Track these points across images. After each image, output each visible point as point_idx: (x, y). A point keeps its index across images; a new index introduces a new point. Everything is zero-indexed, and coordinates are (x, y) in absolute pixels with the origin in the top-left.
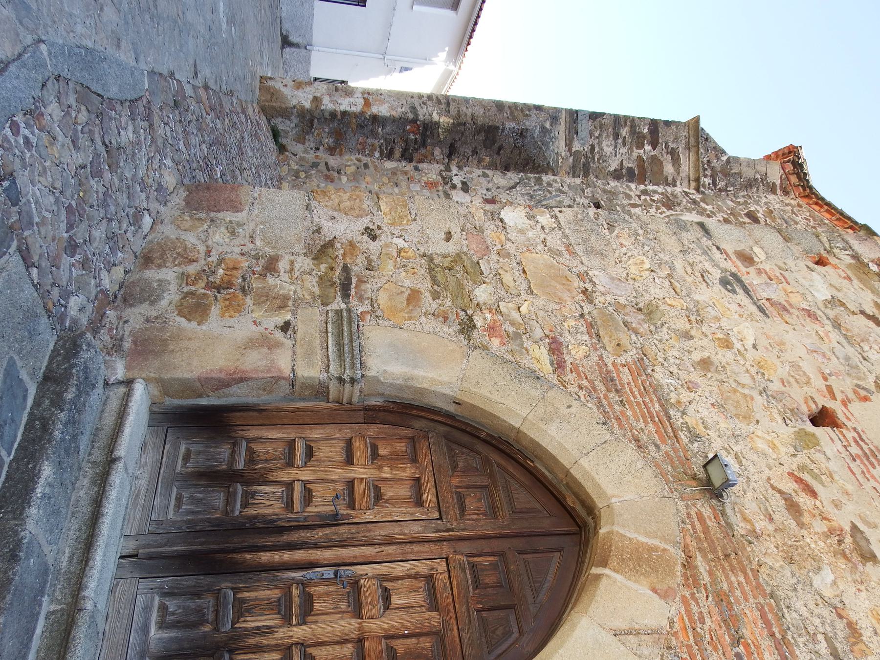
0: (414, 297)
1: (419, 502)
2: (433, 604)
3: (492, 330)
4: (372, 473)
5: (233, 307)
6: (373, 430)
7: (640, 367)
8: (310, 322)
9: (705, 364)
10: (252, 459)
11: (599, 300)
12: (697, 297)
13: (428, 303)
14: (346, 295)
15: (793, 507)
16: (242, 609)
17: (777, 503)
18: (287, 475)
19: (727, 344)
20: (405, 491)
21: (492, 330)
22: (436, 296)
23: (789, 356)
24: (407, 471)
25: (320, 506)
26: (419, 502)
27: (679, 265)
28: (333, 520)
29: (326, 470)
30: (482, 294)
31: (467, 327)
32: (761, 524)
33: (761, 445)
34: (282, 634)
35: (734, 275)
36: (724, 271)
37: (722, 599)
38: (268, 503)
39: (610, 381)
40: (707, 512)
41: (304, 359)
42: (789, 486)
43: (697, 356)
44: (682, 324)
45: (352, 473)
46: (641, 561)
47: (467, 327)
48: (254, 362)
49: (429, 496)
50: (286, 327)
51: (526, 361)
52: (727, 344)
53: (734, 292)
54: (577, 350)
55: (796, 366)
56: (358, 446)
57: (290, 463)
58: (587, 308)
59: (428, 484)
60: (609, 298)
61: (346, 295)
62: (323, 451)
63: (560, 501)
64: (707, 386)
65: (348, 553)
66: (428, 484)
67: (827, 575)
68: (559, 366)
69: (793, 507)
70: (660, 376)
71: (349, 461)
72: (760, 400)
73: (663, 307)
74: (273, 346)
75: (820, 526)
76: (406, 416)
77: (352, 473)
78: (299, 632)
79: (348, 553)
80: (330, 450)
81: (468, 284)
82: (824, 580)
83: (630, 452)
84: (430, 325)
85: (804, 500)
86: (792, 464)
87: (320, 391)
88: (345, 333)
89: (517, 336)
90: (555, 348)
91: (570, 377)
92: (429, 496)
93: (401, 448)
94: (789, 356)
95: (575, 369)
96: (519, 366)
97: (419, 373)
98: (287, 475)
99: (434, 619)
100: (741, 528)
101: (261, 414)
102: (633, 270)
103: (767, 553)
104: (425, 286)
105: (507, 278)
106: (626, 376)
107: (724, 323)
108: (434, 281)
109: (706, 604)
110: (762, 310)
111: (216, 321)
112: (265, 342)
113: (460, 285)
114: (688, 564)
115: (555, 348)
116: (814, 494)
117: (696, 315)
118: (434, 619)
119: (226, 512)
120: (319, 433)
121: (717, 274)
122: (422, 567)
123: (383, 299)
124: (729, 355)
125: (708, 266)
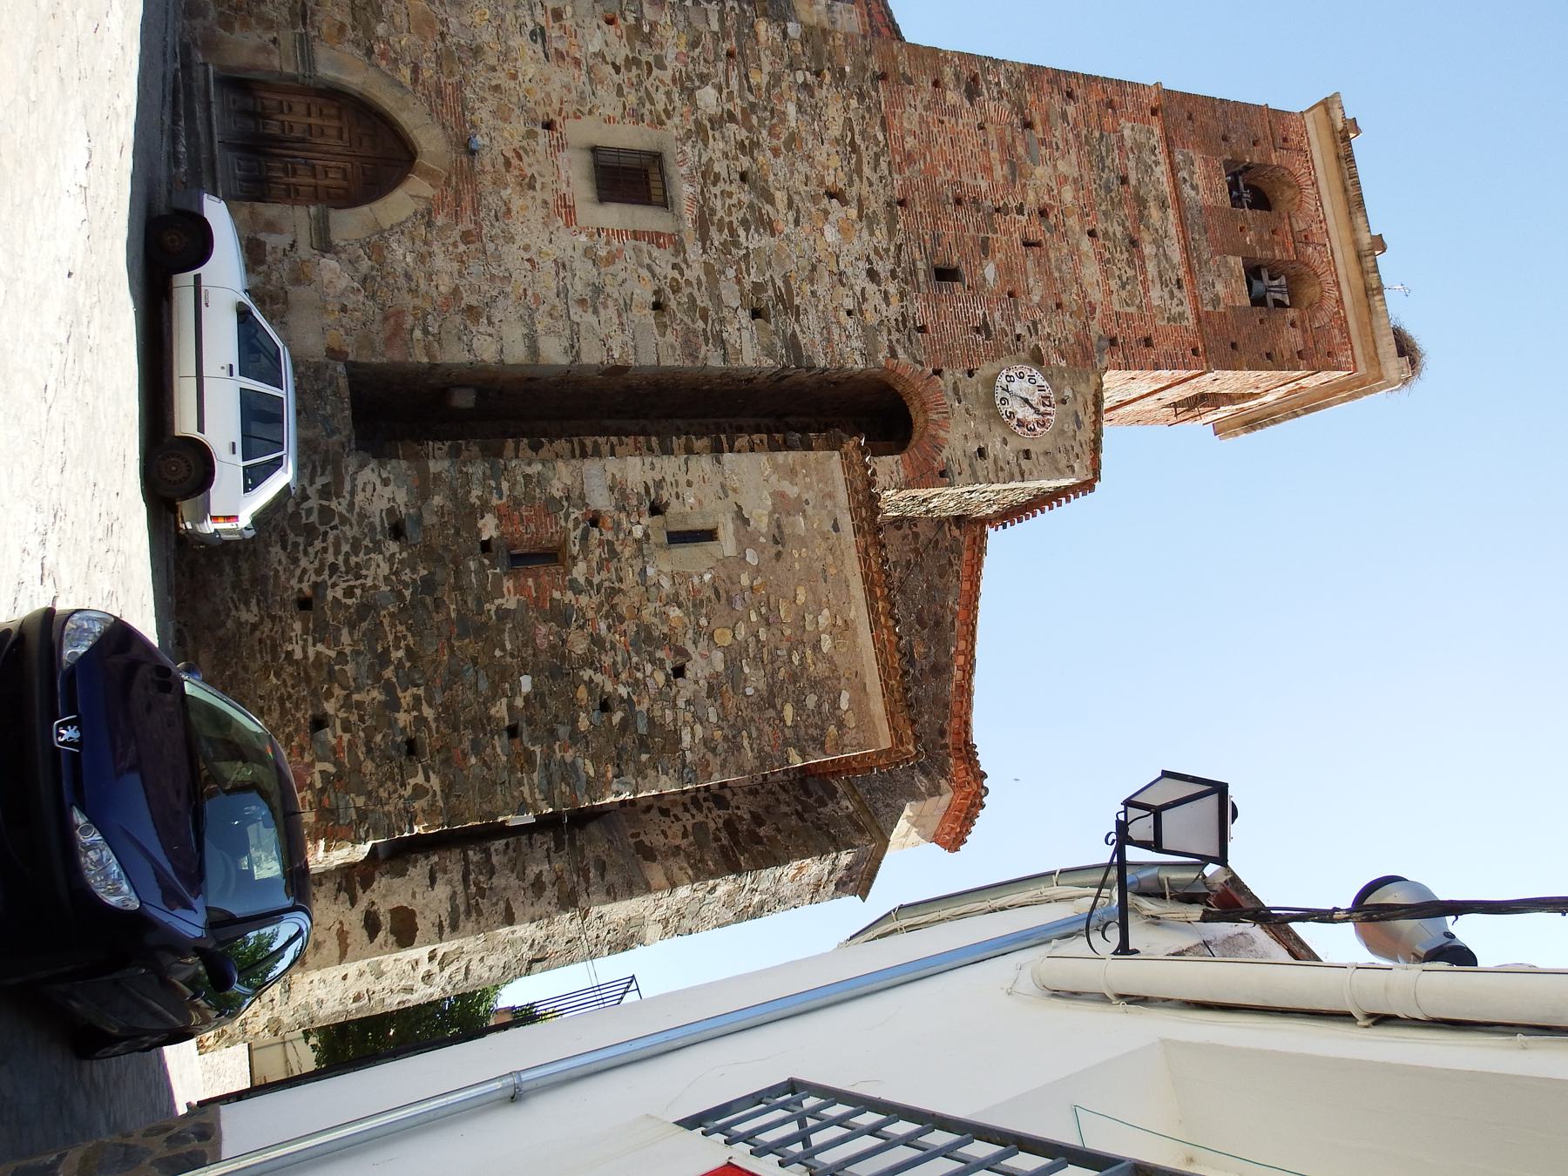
0: (342, 28)
1: (341, 138)
2: (345, 178)
3: (383, 55)
4: (320, 122)
5: (245, 25)
6: (319, 101)
7: (458, 87)
8: (287, 37)
9: (497, 88)
10: (264, 107)
11: (449, 39)
12: (511, 43)
13: (350, 34)
14: (305, 24)
15: (508, 164)
16: (269, 169)
17: (501, 160)
18: (281, 117)
19: (514, 77)
20: (334, 132)
21: (383, 55)
22: (354, 28)
23: (548, 88)
24: (335, 123)
25: (297, 133)
26: (341, 138)
27: (509, 17)
28: (303, 140)
29: (298, 117)
30: (381, 29)
31: (369, 52)
32: (489, 168)
33: (506, 134)
34: (286, 180)
35: (542, 29)
36: (536, 24)
37: (457, 192)
38: (274, 129)
39: (439, 93)
40: (465, 159)
41: (284, 63)
42: (510, 154)
43: (494, 83)
44: (493, 61)
45: (311, 120)
46: (429, 174)
47: (369, 52)
48: (261, 59)
49: (346, 136)
50: (275, 41)
51: (398, 76)
52: (514, 77)
53: (535, 42)
54: (427, 73)
55: (548, 95)
56: (313, 109)
57: (282, 112)
58: (440, 45)
59: (346, 131)
60: (455, 40)
61: (305, 24)
62: (296, 108)
63: (406, 147)
64: (492, 101)
65: (310, 155)
66: (346, 131)
67: (509, 191)
68: (415, 81)
69: (508, 164)
70: (468, 93)
71: (309, 115)
72: (517, 112)
73: (486, 48)
74: (270, 52)
75: (517, 172)
76: (335, 95)
77: (311, 120)
78: (293, 180)
79: (310, 155)
80: (300, 108)
81: (373, 21)
82: (505, 193)
83: (438, 130)
84: (349, 47)
85: (515, 162)
86: (516, 144)
87: (294, 79)
88: (305, 46)
89: (396, 60)
90: (416, 70)
91: (420, 88)
92: (346, 136)
93: (333, 112)
94: (548, 88)
95: (423, 84)
96: (393, 79)
97: (342, 77)
98: (281, 117)
99: (345, 184)
100: (478, 167)
101: (267, 86)
102: (477, 20)
103: (487, 180)
104: (348, 21)
105: (397, 19)
106: (449, 90)
107: (518, 64)
108: (354, 18)
109: (450, 192)
110: (547, 56)
111: (238, 35)
112: (263, 49)
113: (368, 22)
114: (449, 178)
115: (416, 70)
116: (520, 159)
117: (505, 55)
118: (345, 184)
119: (487, 852)
120: (295, 99)
121: (531, 26)
122: (341, 165)
123: (325, 28)
124: (512, 84)
125: (528, 19)
